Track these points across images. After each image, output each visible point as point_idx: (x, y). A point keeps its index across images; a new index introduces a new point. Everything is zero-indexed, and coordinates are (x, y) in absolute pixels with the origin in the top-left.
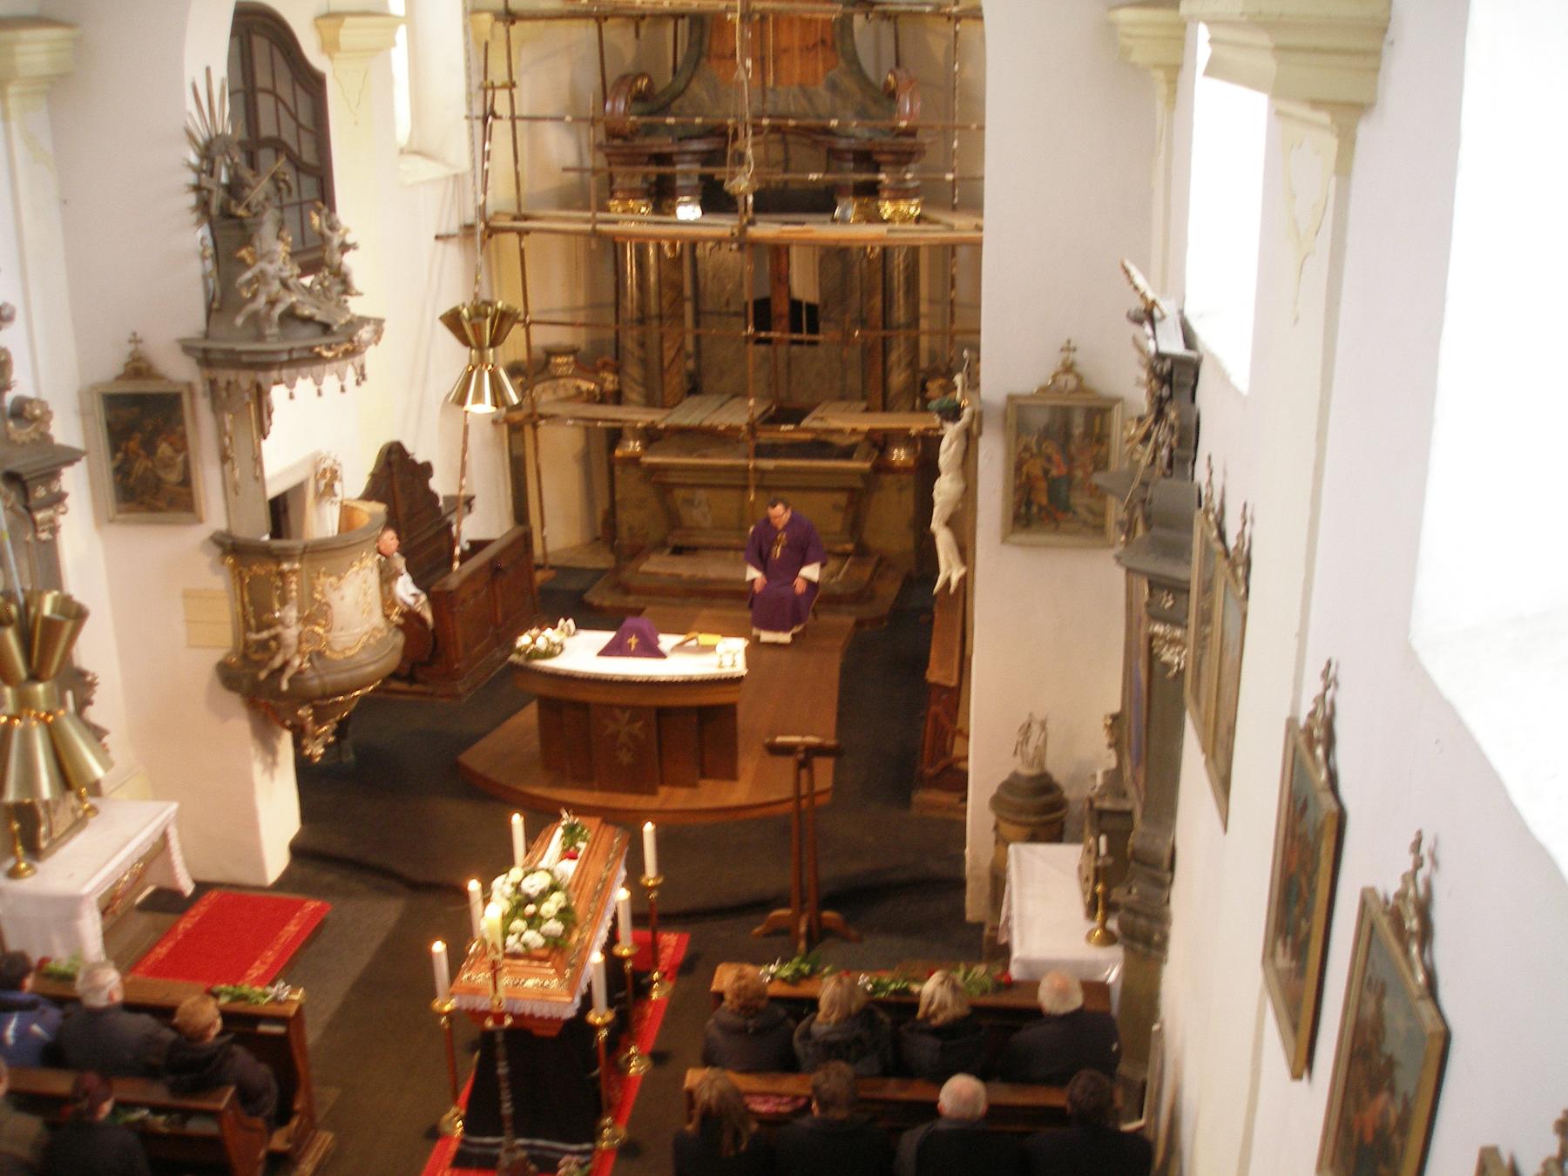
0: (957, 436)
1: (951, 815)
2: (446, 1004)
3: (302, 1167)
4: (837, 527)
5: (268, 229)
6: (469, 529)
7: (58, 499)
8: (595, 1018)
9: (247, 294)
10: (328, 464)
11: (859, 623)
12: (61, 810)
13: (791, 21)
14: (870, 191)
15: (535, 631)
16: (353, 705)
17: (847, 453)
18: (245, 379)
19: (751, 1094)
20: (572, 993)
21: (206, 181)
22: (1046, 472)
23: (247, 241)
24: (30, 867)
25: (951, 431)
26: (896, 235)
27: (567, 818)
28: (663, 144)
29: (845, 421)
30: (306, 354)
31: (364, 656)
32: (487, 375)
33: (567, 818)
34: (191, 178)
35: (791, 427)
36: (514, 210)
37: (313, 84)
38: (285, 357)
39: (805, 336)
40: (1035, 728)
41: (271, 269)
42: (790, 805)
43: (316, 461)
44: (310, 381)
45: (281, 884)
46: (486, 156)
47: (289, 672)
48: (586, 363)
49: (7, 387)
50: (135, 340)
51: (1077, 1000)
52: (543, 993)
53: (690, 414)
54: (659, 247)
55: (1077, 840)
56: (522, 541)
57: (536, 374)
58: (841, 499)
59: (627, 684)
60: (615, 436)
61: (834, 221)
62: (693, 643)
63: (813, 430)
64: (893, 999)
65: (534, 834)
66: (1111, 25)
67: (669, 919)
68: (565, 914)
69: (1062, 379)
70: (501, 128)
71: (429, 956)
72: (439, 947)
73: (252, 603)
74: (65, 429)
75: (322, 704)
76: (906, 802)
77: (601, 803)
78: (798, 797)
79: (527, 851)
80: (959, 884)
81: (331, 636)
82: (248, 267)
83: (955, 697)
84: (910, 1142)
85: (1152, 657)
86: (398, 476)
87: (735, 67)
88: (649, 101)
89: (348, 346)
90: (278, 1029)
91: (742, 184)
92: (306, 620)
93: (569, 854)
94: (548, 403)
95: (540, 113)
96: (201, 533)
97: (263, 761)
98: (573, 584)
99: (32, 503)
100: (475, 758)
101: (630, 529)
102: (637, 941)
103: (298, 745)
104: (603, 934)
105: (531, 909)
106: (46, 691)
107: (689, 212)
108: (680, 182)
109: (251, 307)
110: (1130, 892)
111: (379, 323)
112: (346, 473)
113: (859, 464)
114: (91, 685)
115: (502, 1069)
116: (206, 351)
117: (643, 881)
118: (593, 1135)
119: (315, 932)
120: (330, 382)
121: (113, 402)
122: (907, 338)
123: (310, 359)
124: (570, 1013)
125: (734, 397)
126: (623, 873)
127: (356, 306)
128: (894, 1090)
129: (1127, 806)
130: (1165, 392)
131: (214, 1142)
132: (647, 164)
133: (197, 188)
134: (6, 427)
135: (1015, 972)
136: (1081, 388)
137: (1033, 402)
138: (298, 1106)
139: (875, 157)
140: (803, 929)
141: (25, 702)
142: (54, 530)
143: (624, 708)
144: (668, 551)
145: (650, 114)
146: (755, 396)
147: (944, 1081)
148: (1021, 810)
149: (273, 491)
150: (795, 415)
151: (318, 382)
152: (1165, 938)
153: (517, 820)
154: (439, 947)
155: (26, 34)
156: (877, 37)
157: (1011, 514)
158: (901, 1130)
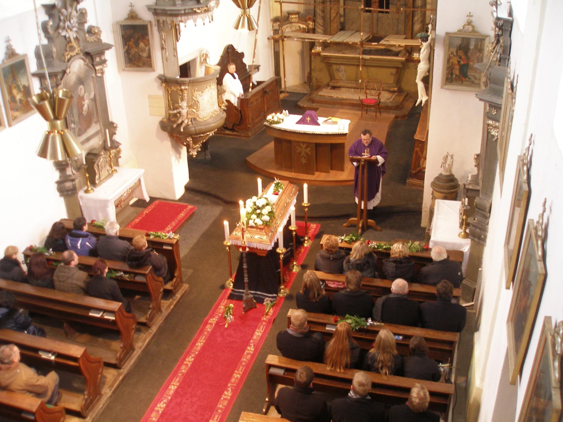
0: (427, 48)
1: (420, 189)
2: (228, 243)
3: (177, 295)
4: (392, 82)
6: (256, 77)
7: (104, 62)
8: (278, 250)
10: (204, 52)
12: (103, 170)
15: (274, 114)
16: (207, 138)
17: (397, 54)
18: (169, 20)
19: (328, 280)
20: (271, 241)
22: (459, 62)
24: (92, 189)
25: (425, 44)
27: (277, 181)
29: (397, 42)
30: (190, 11)
31: (211, 120)
32: (246, 18)
33: (277, 181)
38: (183, 12)
39: (384, 10)
40: (449, 158)
44: (192, 21)
45: (180, 200)
47: (184, 125)
48: (303, 18)
49: (86, 22)
50: (131, 6)
51: (445, 256)
52: (262, 241)
53: (340, 38)
55: (460, 200)
56: (277, 82)
57: (284, 21)
60: (312, 45)
62: (330, 121)
63: (384, 45)
64: (384, 251)
65: (265, 186)
67: (313, 219)
68: (271, 214)
69: (467, 27)
71: (223, 227)
73: (171, 100)
74: (108, 36)
76: (405, 183)
77: (294, 177)
80: (420, 213)
81: (198, 113)
83: (423, 145)
84: (380, 301)
85: (488, 133)
89: (206, 8)
90: (170, 248)
92: (190, 107)
94: (288, 32)
97: (176, 157)
98: (294, 99)
99: (95, 63)
100: (251, 159)
101: (316, 79)
102: (297, 224)
104: (285, 222)
105: (258, 211)
110: (474, 219)
114: (116, 128)
115: (245, 266)
116: (155, 10)
118: (277, 291)
119: (191, 215)
122: (421, 11)
124: (270, 248)
125: (357, 32)
126: (295, 201)
128: (379, 283)
129: (478, 188)
131: (144, 284)
134: (85, 36)
136: (474, 31)
138: (176, 275)
140: (360, 225)
142: (103, 73)
143: (304, 143)
144: (330, 88)
146: (363, 32)
147: (393, 281)
148: (442, 188)
149: (181, 62)
150: (377, 39)
151: (195, 21)
152: (486, 237)
153: (259, 181)
154: (226, 223)
158: (377, 297)
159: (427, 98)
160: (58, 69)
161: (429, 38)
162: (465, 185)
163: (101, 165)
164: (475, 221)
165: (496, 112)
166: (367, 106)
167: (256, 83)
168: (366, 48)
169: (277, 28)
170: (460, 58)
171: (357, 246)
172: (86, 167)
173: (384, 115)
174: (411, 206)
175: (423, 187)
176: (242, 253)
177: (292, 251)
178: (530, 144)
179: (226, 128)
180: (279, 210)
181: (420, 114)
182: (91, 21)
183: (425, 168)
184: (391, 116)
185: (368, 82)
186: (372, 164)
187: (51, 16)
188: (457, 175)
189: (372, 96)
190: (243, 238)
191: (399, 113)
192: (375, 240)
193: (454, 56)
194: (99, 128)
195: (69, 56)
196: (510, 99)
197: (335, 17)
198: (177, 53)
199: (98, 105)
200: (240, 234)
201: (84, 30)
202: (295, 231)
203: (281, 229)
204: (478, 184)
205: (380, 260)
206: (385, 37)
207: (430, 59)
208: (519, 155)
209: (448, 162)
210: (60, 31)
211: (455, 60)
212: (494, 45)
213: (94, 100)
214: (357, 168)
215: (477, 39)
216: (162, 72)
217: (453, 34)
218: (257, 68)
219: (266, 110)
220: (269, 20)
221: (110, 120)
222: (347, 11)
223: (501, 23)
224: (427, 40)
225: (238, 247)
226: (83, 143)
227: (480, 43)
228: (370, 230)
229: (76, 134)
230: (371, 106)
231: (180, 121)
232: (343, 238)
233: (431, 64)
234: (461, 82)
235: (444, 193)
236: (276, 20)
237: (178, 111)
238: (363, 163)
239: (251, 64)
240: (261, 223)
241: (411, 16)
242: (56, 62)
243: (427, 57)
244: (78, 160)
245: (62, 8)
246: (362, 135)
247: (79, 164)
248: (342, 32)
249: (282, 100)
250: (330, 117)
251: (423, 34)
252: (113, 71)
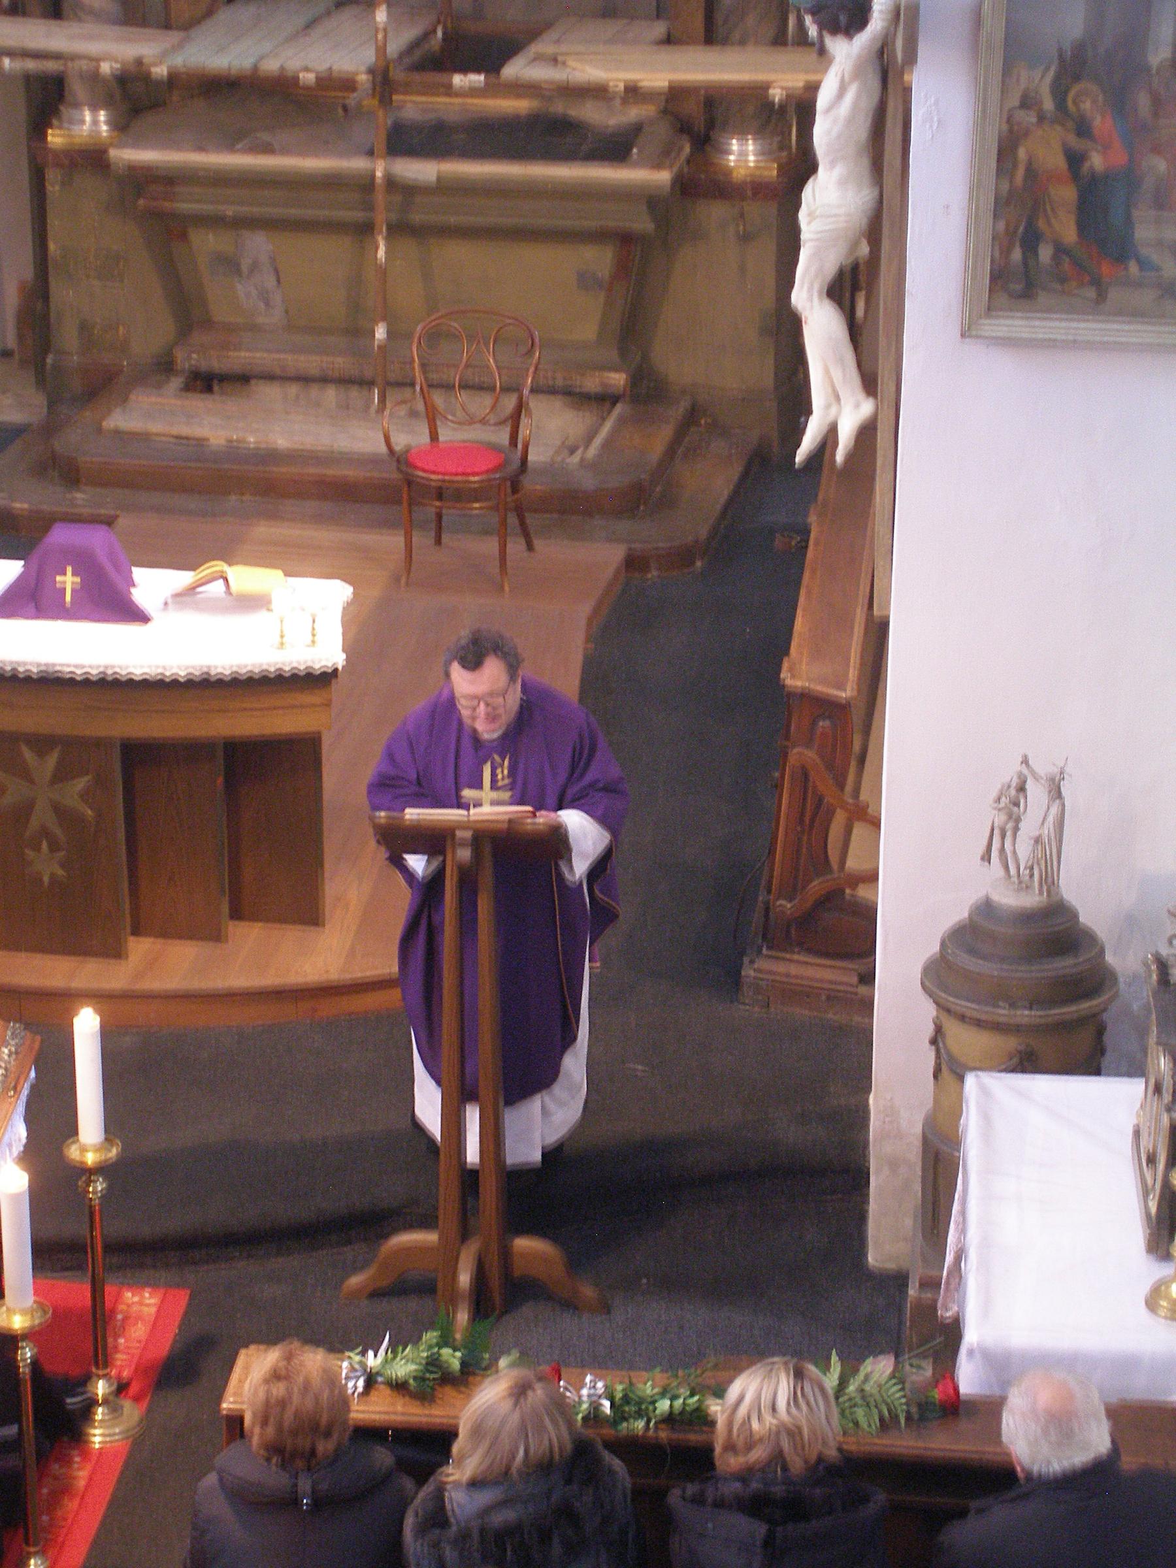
0: (858, 72)
4: (588, 331)
11: (634, 563)
17: (615, 148)
22: (1075, 160)
35: (477, 79)
40: (1036, 793)
51: (1097, 1441)
55: (1135, 1069)
59: (50, 685)
62: (218, 587)
64: (664, 1435)
67: (139, 1254)
80: (856, 1179)
83: (849, 728)
101: (84, 328)
113: (643, 175)
135: (969, 1378)
140: (465, 1279)
143: (42, 743)
144: (176, 382)
148: (1000, 994)
150: (487, 52)
159: (867, 408)
166: (440, 494)
171: (489, 1410)
173: (555, 550)
174: (790, 1132)
175: (867, 1005)
181: (805, 532)
184: (600, 555)
185: (434, 336)
186: (526, 859)
188: (1094, 908)
189: (467, 431)
191: (653, 535)
192: (600, 1363)
193: (1041, 118)
205: (651, 1501)
206: (534, 34)
209: (1029, 826)
211: (1047, 150)
214: (429, 891)
228: (527, 1310)
230: (459, 495)
232: (373, 1361)
233: (890, 179)
234: (1091, 293)
238: (464, 854)
243: (862, 131)
246: (458, 674)
250: (220, 566)
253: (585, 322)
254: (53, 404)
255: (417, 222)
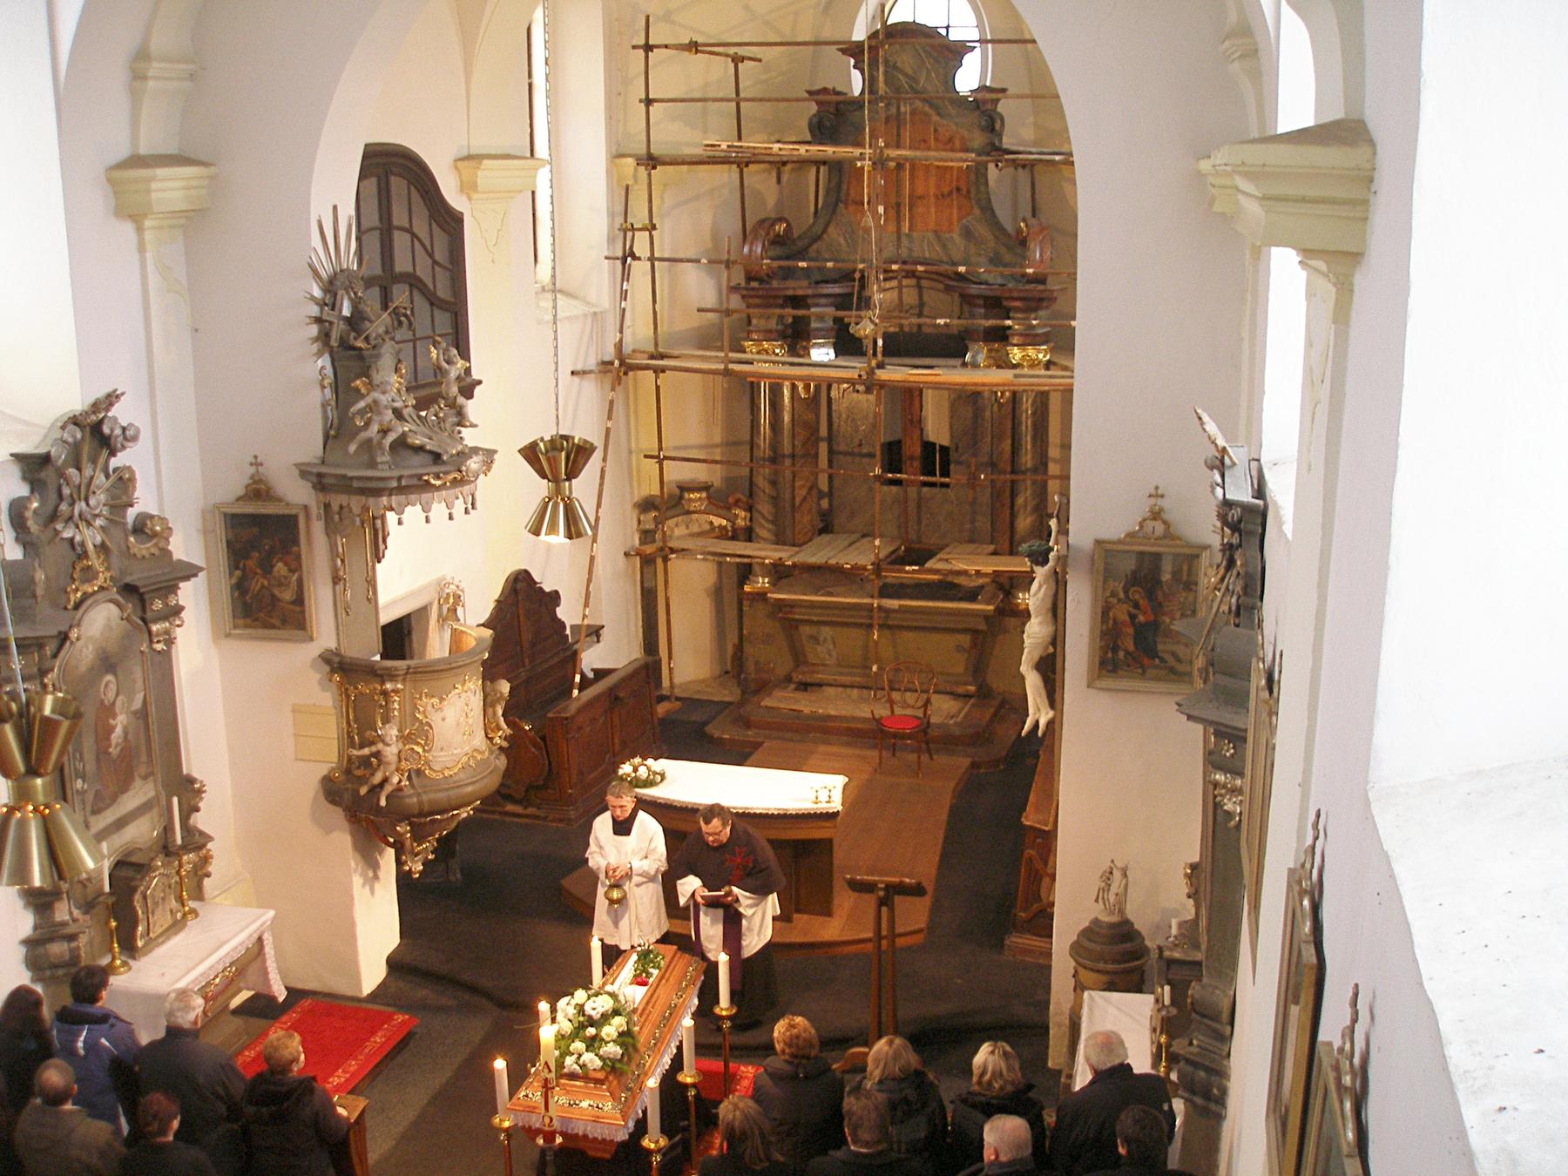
0: (1046, 580)
4: (961, 669)
5: (387, 361)
6: (591, 658)
7: (178, 610)
9: (360, 423)
11: (974, 765)
13: (927, 167)
14: (1000, 336)
15: (637, 760)
16: (453, 825)
17: (972, 595)
18: (356, 503)
21: (328, 314)
22: (1133, 617)
23: (365, 372)
24: (125, 964)
25: (1041, 572)
26: (1023, 380)
28: (800, 287)
29: (973, 564)
30: (415, 482)
31: (462, 776)
34: (314, 310)
36: (651, 349)
37: (450, 223)
38: (394, 484)
39: (938, 479)
40: (1117, 874)
41: (384, 399)
42: (870, 946)
43: (442, 584)
44: (419, 507)
45: (374, 996)
46: (624, 295)
47: (388, 789)
48: (719, 499)
50: (256, 463)
52: (597, 1115)
54: (794, 387)
56: (649, 671)
58: (965, 640)
60: (745, 571)
61: (964, 365)
63: (937, 572)
66: (1200, 175)
68: (625, 1037)
69: (1150, 524)
70: (640, 269)
71: (491, 1075)
72: (500, 1064)
74: (185, 545)
75: (421, 820)
76: (1000, 946)
78: (879, 936)
79: (604, 974)
82: (363, 397)
83: (1046, 840)
86: (525, 602)
87: (863, 213)
88: (786, 245)
91: (865, 328)
92: (405, 738)
93: (639, 981)
95: (681, 255)
96: (313, 650)
97: (364, 875)
98: (696, 717)
99: (149, 615)
101: (757, 663)
103: (399, 863)
104: (666, 1061)
105: (591, 1031)
106: (44, 785)
107: (822, 353)
108: (814, 325)
109: (364, 435)
110: (1191, 1044)
111: (490, 454)
112: (467, 599)
116: (320, 475)
117: (717, 1010)
120: (438, 509)
121: (235, 521)
122: (1034, 482)
123: (418, 487)
124: (622, 1136)
125: (864, 536)
127: (470, 437)
129: (1199, 956)
130: (1235, 540)
132: (782, 307)
133: (318, 320)
136: (1168, 535)
137: (1121, 547)
139: (1005, 303)
141: (22, 795)
142: (170, 642)
145: (787, 258)
146: (881, 536)
149: (386, 617)
150: (918, 555)
152: (1224, 1092)
154: (500, 1064)
155: (161, 172)
156: (1015, 187)
157: (1097, 660)
159: (1051, 714)
160: (47, 629)
161: (1052, 555)
162: (1160, 949)
163: (153, 896)
164: (1194, 1050)
165: (1234, 751)
166: (895, 736)
167: (591, 675)
168: (889, 580)
169: (650, 526)
170: (1136, 605)
172: (110, 901)
173: (942, 759)
176: (543, 1151)
177: (685, 1144)
178: (1316, 838)
179: (509, 798)
180: (648, 1026)
181: (1038, 757)
182: (144, 501)
183: (1053, 904)
187: (35, 484)
189: (906, 707)
190: (547, 1108)
194: (152, 794)
195: (79, 594)
196: (1264, 715)
197: (805, 499)
198: (375, 593)
199: (154, 728)
200: (537, 1097)
201: (125, 524)
202: (694, 1085)
203: (653, 1082)
204: (1197, 946)
207: (1056, 610)
208: (1292, 866)
209: (1114, 889)
210: (59, 527)
211: (1121, 613)
212: (1222, 571)
213: (143, 714)
215: (1177, 555)
216: (333, 645)
217: (1114, 543)
218: (595, 632)
219: (617, 747)
220: (629, 506)
221: (185, 772)
222: (837, 482)
223: (1236, 513)
224: (1046, 561)
225: (532, 1133)
226: (100, 836)
227: (1185, 568)
229: (88, 809)
230: (904, 737)
231: (378, 778)
233: (1060, 621)
235: (1107, 972)
236: (646, 505)
237: (374, 749)
239: (578, 621)
240: (598, 1063)
241: (1008, 494)
242: (44, 609)
243: (1049, 604)
244: (89, 880)
245: (66, 464)
247: (90, 890)
248: (826, 538)
249: (662, 721)
251: (1036, 544)
252: (197, 644)
253: (959, 665)
254: (743, 693)
255: (890, 622)
